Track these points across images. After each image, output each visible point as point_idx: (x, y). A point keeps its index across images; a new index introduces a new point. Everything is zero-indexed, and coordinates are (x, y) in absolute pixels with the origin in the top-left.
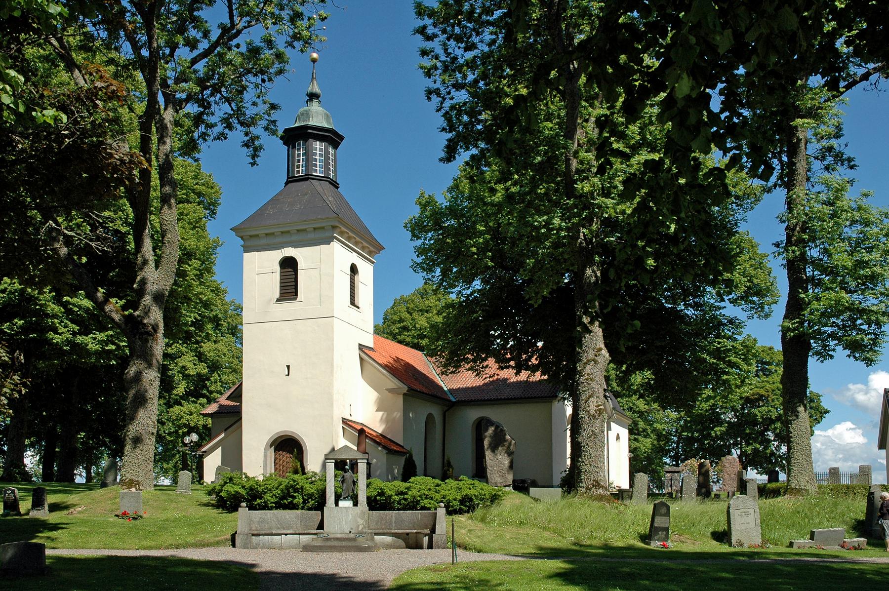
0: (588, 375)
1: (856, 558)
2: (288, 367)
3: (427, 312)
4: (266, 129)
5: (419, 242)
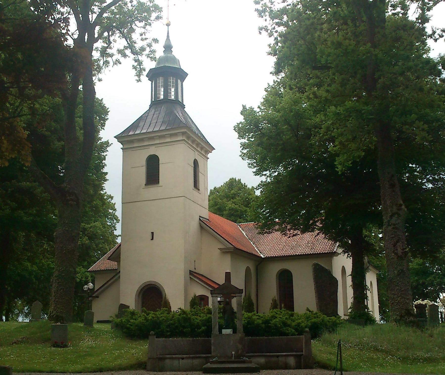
0: (394, 225)
1: (190, 361)
2: (153, 233)
3: (233, 198)
4: (148, 56)
5: (243, 141)
